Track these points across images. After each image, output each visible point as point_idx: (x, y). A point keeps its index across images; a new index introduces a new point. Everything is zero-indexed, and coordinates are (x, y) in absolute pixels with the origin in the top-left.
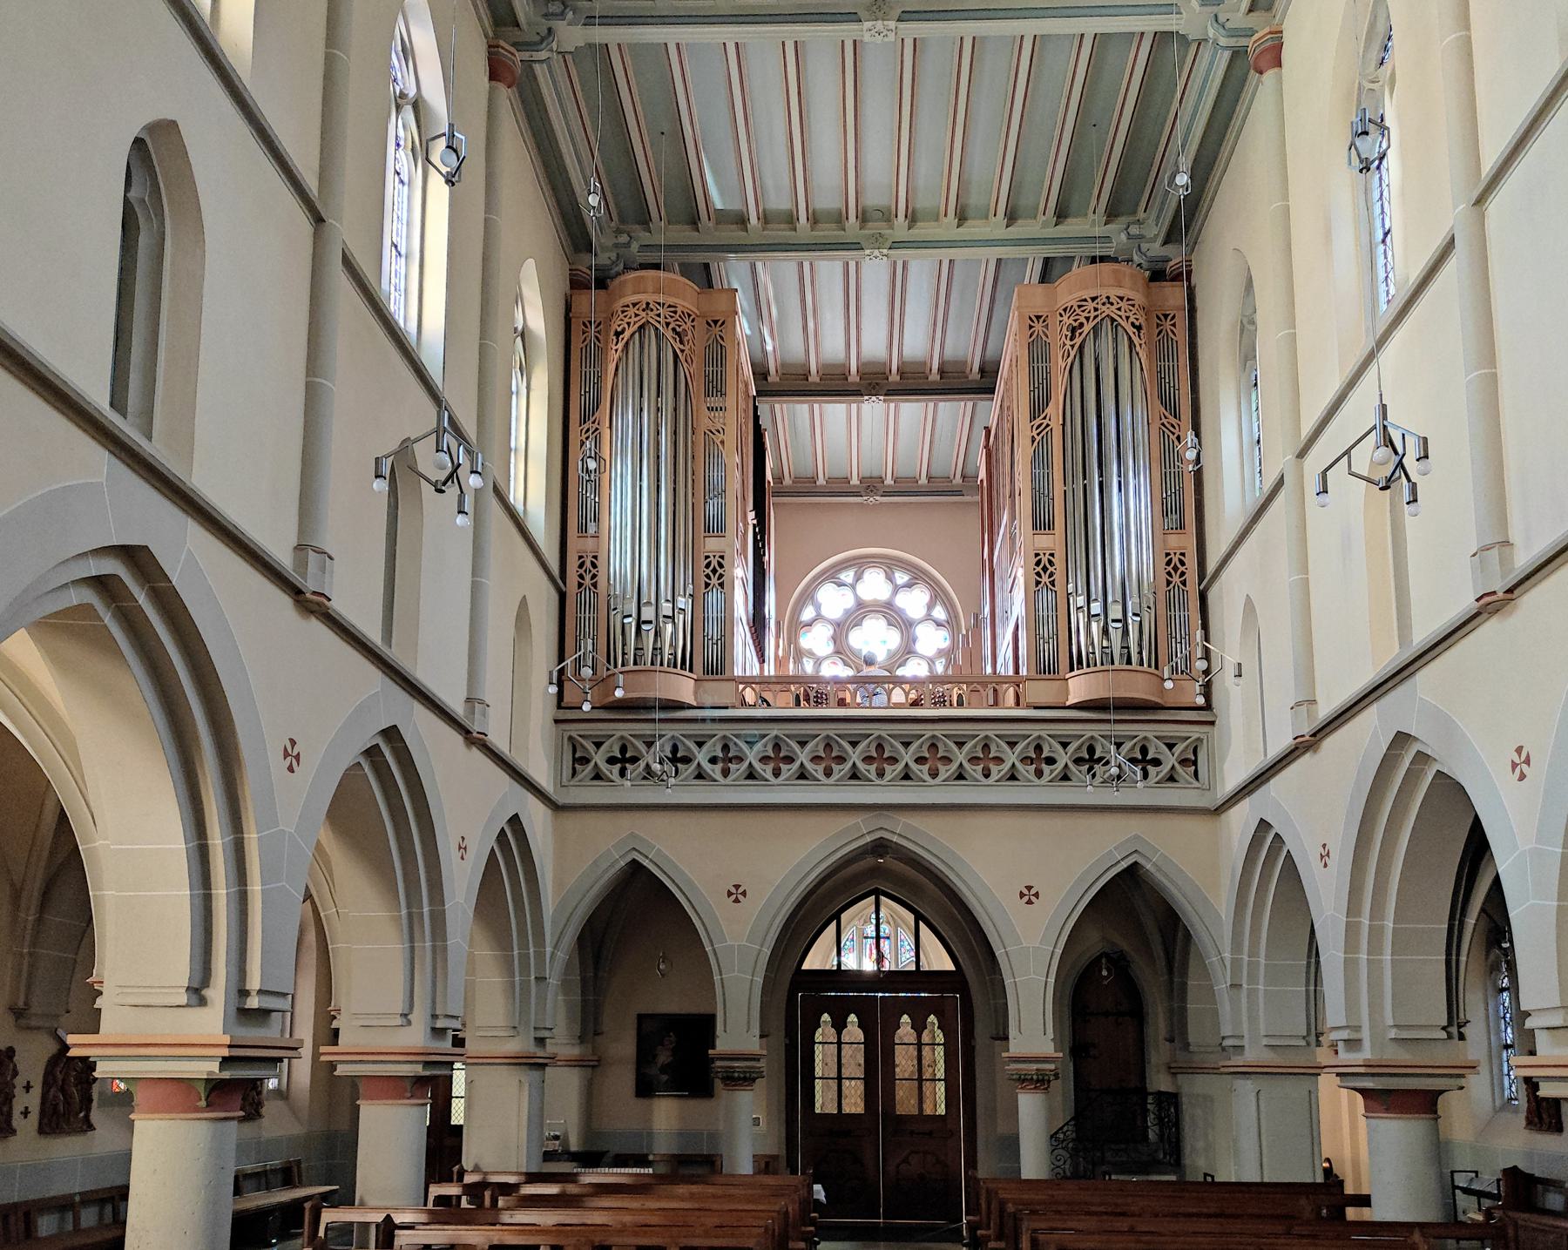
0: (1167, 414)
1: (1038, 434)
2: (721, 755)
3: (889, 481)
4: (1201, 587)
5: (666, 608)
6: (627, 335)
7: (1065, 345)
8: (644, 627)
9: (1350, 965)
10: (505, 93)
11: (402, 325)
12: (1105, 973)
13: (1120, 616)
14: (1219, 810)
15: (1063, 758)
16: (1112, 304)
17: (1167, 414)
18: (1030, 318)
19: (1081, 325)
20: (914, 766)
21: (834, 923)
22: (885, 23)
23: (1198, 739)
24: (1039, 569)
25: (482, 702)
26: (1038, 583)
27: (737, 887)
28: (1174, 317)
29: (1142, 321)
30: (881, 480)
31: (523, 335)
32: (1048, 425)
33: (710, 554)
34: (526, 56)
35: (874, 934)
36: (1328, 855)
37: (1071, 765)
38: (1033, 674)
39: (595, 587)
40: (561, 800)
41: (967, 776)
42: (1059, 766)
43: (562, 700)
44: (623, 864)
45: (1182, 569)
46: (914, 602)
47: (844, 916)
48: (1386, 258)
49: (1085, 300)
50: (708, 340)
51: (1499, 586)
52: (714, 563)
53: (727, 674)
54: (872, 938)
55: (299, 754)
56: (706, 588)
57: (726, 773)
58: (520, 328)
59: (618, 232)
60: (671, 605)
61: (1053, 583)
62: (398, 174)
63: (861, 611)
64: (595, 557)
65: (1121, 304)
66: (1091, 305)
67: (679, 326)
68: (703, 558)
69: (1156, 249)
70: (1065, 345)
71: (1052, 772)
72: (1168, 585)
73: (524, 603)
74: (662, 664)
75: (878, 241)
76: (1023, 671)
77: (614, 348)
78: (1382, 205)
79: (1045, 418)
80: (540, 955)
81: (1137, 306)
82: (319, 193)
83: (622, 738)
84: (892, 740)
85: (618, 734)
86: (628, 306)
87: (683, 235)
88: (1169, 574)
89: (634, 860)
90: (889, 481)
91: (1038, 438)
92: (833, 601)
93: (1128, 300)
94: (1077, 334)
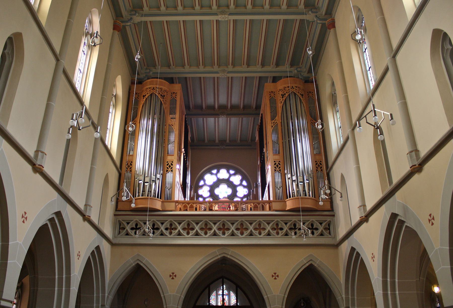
0: (313, 120)
1: (274, 125)
2: (169, 227)
3: (228, 141)
4: (327, 172)
5: (153, 177)
6: (146, 97)
7: (280, 99)
8: (146, 184)
9: (385, 296)
10: (116, 32)
11: (79, 91)
12: (302, 305)
13: (302, 181)
14: (337, 246)
15: (286, 228)
16: (294, 88)
17: (313, 120)
18: (270, 92)
19: (285, 94)
20: (235, 231)
21: (208, 289)
22: (225, 16)
23: (330, 221)
24: (275, 166)
25: (90, 206)
26: (275, 170)
27: (173, 273)
28: (312, 93)
29: (303, 93)
30: (225, 141)
31: (115, 96)
32: (276, 122)
33: (169, 161)
34: (124, 24)
35: (222, 294)
36: (374, 257)
37: (288, 230)
38: (275, 200)
39: (131, 172)
40: (114, 242)
41: (253, 235)
42: (284, 231)
43: (117, 208)
44: (134, 265)
45: (321, 166)
46: (236, 179)
47: (211, 287)
48: (370, 74)
49: (286, 87)
50: (171, 98)
51: (416, 163)
52: (170, 164)
53: (172, 200)
54: (221, 295)
55: (27, 217)
56: (167, 172)
57: (171, 233)
58: (115, 94)
59: (146, 69)
60: (155, 177)
61: (280, 170)
62: (84, 52)
63: (219, 182)
64: (132, 162)
65: (296, 89)
66: (287, 89)
67: (163, 94)
68: (166, 162)
69: (306, 75)
70: (280, 99)
71: (282, 233)
72: (317, 171)
73: (107, 176)
74: (151, 196)
75: (222, 114)
76: (271, 199)
77: (143, 100)
78: (367, 61)
79: (275, 120)
80: (103, 297)
81: (301, 89)
82: (60, 52)
83: (136, 221)
84: (228, 222)
85: (135, 220)
86: (147, 88)
87: (166, 70)
88: (317, 167)
89: (138, 264)
90: (228, 141)
91: (274, 126)
92: (210, 179)
93: (299, 87)
94: (284, 97)
